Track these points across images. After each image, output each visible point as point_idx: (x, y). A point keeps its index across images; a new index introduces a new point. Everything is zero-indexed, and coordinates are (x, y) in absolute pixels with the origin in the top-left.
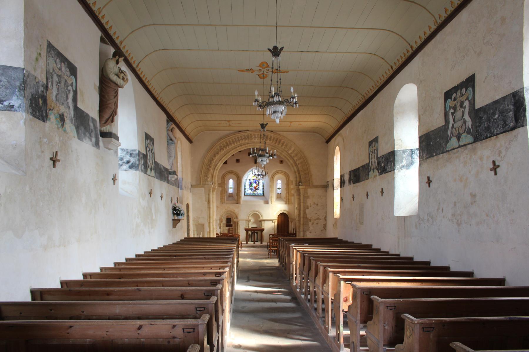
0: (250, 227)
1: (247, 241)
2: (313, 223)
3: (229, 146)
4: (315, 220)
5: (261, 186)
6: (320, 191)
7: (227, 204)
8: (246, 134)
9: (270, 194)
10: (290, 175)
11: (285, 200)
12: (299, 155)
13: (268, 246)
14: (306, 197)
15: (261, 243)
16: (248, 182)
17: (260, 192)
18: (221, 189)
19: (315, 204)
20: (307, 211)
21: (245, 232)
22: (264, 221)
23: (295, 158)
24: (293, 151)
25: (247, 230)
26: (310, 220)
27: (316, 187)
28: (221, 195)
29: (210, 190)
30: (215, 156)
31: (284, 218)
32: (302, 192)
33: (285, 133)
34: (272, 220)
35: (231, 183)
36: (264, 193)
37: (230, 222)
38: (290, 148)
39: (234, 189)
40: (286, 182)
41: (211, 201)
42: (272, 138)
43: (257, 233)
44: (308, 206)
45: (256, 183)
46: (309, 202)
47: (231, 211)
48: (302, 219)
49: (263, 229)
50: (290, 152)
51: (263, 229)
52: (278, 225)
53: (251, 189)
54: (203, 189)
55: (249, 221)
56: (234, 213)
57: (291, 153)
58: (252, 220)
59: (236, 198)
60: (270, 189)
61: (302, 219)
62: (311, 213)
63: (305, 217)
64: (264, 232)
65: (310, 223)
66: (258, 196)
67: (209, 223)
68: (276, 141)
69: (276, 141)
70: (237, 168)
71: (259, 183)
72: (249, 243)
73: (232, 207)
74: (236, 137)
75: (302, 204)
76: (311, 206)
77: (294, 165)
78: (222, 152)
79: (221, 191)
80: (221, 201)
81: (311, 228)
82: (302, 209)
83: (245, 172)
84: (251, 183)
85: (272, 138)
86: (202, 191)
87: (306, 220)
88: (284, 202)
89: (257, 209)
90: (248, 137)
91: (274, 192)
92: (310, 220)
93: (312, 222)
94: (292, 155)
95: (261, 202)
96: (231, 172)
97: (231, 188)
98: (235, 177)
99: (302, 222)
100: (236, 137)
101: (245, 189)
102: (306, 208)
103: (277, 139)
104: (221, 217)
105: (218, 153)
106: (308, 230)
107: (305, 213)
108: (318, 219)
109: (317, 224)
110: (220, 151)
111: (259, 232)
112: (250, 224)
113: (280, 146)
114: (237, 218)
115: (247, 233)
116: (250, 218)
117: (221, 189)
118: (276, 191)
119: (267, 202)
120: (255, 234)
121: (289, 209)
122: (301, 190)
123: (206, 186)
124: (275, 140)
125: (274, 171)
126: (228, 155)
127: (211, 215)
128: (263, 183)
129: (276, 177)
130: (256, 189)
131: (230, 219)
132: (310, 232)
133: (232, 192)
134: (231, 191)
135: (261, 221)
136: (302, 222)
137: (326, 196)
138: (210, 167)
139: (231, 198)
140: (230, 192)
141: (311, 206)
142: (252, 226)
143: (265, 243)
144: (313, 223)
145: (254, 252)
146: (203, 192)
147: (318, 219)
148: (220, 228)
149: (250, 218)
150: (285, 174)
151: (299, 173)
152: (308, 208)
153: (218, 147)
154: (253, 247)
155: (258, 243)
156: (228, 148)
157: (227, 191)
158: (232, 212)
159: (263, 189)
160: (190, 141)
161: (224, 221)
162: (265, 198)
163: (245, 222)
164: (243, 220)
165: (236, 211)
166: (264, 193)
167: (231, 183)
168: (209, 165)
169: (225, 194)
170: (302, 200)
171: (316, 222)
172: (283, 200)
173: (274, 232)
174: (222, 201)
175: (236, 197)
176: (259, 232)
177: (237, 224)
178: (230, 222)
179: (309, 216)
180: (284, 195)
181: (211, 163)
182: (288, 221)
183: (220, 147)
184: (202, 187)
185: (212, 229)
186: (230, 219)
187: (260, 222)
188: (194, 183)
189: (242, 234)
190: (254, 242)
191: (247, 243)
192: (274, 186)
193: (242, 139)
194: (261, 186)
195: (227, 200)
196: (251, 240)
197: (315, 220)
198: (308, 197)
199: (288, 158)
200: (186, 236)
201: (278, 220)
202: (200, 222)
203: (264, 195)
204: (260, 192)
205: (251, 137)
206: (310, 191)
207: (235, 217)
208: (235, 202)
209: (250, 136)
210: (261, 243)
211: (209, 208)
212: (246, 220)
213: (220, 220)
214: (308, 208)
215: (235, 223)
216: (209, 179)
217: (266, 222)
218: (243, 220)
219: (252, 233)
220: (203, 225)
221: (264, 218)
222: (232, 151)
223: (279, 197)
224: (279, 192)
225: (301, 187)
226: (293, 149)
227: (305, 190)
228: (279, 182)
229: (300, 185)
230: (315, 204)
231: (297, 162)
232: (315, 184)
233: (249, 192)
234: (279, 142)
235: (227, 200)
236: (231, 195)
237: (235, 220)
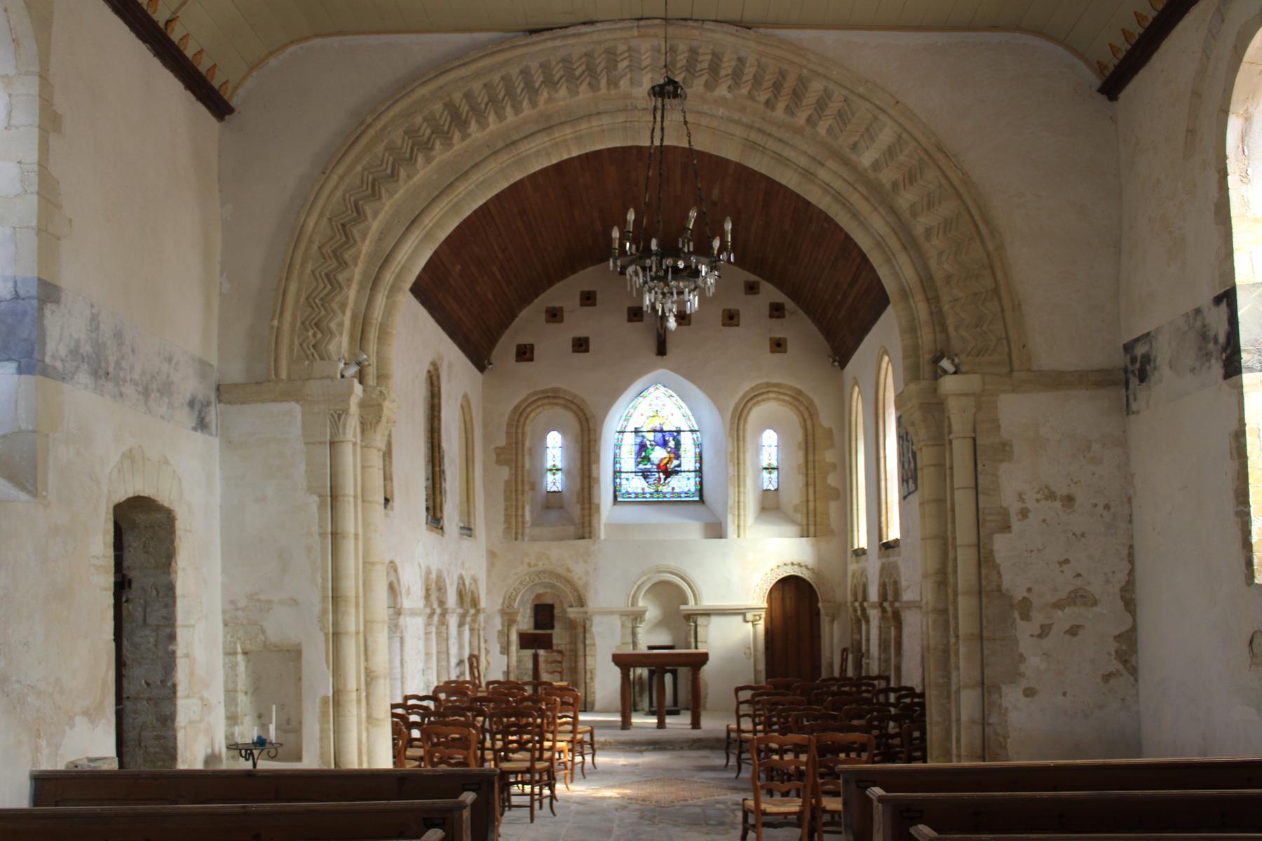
0: (642, 649)
1: (628, 707)
2: (1045, 631)
3: (462, 124)
4: (1058, 605)
5: (688, 461)
6: (1082, 412)
7: (534, 539)
8: (575, 45)
9: (732, 492)
10: (817, 401)
11: (800, 517)
12: (931, 174)
13: (730, 744)
14: (987, 451)
15: (696, 724)
16: (630, 441)
17: (683, 484)
18: (505, 472)
19: (1051, 496)
20: (1002, 546)
21: (616, 672)
22: (707, 614)
23: (905, 200)
24: (890, 152)
25: (624, 662)
26: (1025, 608)
27: (1057, 381)
28: (507, 499)
29: (338, 417)
30: (375, 195)
31: (795, 599)
32: (959, 418)
33: (831, 37)
34: (741, 612)
35: (555, 447)
36: (701, 492)
37: (548, 624)
38: (869, 134)
39: (568, 474)
40: (800, 436)
41: (349, 486)
42: (750, 71)
43: (674, 673)
44: (1005, 514)
45: (665, 444)
46: (1013, 483)
47: (554, 574)
48: (965, 604)
49: (704, 658)
50: (866, 160)
51: (704, 658)
52: (769, 632)
53: (645, 475)
54: (296, 408)
55: (637, 617)
56: (569, 582)
57: (876, 166)
58: (653, 614)
59: (576, 512)
60: (732, 470)
61: (965, 604)
62: (1024, 560)
63: (988, 588)
64: (707, 670)
65: (1024, 631)
66: (676, 502)
67: (337, 636)
68: (777, 87)
69: (777, 87)
70: (577, 377)
71: (678, 444)
72: (636, 720)
73: (560, 555)
74: (514, 71)
75: (963, 501)
76: (1024, 513)
77: (893, 243)
78: (423, 172)
79: (507, 483)
80: (508, 528)
81: (1034, 662)
82: (964, 532)
83: (614, 394)
84: (642, 447)
85: (750, 71)
86: (285, 421)
87: (998, 607)
88: (793, 529)
89: (672, 563)
90: (591, 70)
91: (749, 482)
92: (1025, 608)
93: (1038, 618)
94: (887, 176)
95: (690, 529)
96: (552, 397)
97: (555, 470)
98: (568, 417)
99: (966, 625)
100: (514, 71)
101: (617, 473)
102: (992, 523)
103: (783, 75)
104: (509, 599)
105: (394, 176)
106: (1014, 676)
107: (984, 559)
108: (1080, 597)
109: (1073, 631)
110: (411, 160)
111: (684, 672)
112: (641, 630)
113: (801, 119)
114: (581, 602)
115: (625, 676)
116: (641, 603)
117: (505, 472)
118: (757, 478)
119: (716, 530)
120: (666, 677)
121: (820, 557)
122: (953, 406)
123: (313, 388)
124: (768, 80)
125: (746, 386)
126: (461, 189)
127: (351, 586)
128: (699, 446)
129: (757, 413)
130: (668, 474)
131: (551, 607)
132: (1029, 693)
133: (558, 487)
134: (554, 482)
135: (690, 617)
136: (966, 625)
137: (1122, 442)
138: (343, 265)
139: (553, 515)
140: (551, 488)
141: (1024, 513)
142: (649, 638)
143: (714, 724)
144: (1045, 631)
145: (654, 791)
146: (296, 431)
147: (1080, 597)
148: (505, 650)
149: (641, 603)
150: (798, 400)
151: (933, 300)
152: (1006, 528)
153: (397, 135)
154: (655, 745)
155: (679, 724)
156: (458, 145)
157: (535, 485)
158: (558, 576)
159: (699, 472)
160: (218, 105)
161: (525, 622)
162: (707, 512)
163: (616, 621)
164: (611, 613)
165: (578, 571)
166: (701, 492)
167: (555, 447)
168: (337, 254)
169: (528, 497)
170: (962, 475)
171: (1064, 619)
172: (793, 521)
173: (750, 672)
174: (514, 528)
175: (576, 511)
176: (684, 672)
177: (579, 630)
178: (548, 624)
179: (1015, 583)
180: (793, 496)
181: (349, 241)
182: (816, 614)
183: (411, 132)
184: (286, 396)
185: (353, 680)
186: (551, 607)
187: (684, 616)
188: (236, 372)
189: (605, 682)
190: (660, 712)
191: (626, 724)
192: (749, 456)
193: (551, 83)
194: (688, 461)
195: (535, 524)
196: (645, 704)
197: (1058, 605)
198: (1004, 450)
199: (855, 199)
200: (93, 744)
201: (770, 611)
202: (273, 636)
203: (702, 500)
204: (683, 484)
205: (612, 64)
206: (1017, 411)
207: (572, 598)
208: (571, 529)
209: (601, 63)
210: (696, 724)
211: (336, 536)
212: (623, 614)
213: (503, 613)
214: (1006, 528)
215: (571, 625)
216: (341, 344)
217: (715, 620)
218: (611, 613)
219: (651, 673)
220: (294, 654)
221: (708, 602)
222: (492, 167)
223: (770, 506)
224: (770, 481)
225: (949, 384)
226: (886, 136)
227: (982, 402)
228: (770, 438)
229: (938, 374)
230: (1051, 496)
231: (919, 226)
232: (1048, 358)
233: (635, 485)
234: (797, 96)
235: (535, 524)
236: (553, 502)
237: (573, 612)
